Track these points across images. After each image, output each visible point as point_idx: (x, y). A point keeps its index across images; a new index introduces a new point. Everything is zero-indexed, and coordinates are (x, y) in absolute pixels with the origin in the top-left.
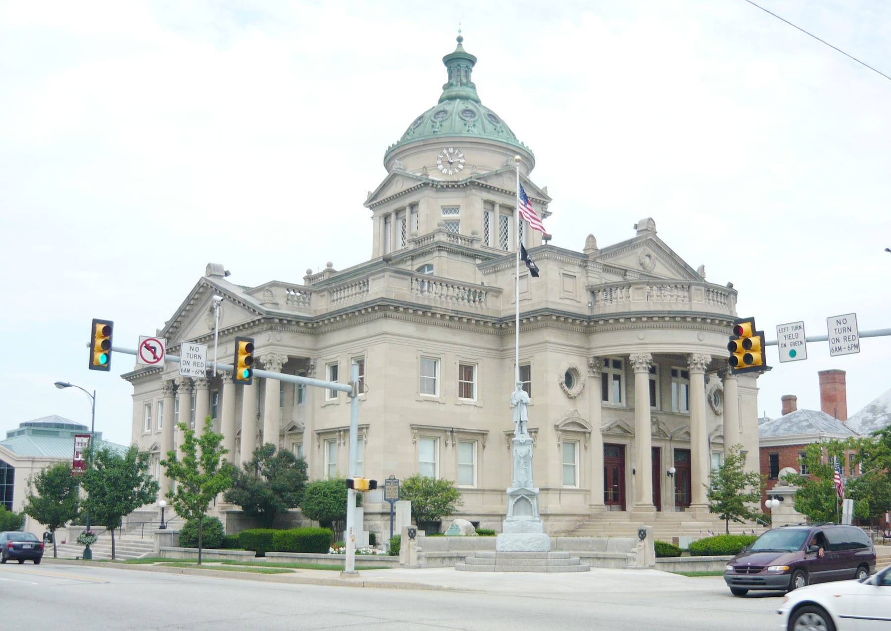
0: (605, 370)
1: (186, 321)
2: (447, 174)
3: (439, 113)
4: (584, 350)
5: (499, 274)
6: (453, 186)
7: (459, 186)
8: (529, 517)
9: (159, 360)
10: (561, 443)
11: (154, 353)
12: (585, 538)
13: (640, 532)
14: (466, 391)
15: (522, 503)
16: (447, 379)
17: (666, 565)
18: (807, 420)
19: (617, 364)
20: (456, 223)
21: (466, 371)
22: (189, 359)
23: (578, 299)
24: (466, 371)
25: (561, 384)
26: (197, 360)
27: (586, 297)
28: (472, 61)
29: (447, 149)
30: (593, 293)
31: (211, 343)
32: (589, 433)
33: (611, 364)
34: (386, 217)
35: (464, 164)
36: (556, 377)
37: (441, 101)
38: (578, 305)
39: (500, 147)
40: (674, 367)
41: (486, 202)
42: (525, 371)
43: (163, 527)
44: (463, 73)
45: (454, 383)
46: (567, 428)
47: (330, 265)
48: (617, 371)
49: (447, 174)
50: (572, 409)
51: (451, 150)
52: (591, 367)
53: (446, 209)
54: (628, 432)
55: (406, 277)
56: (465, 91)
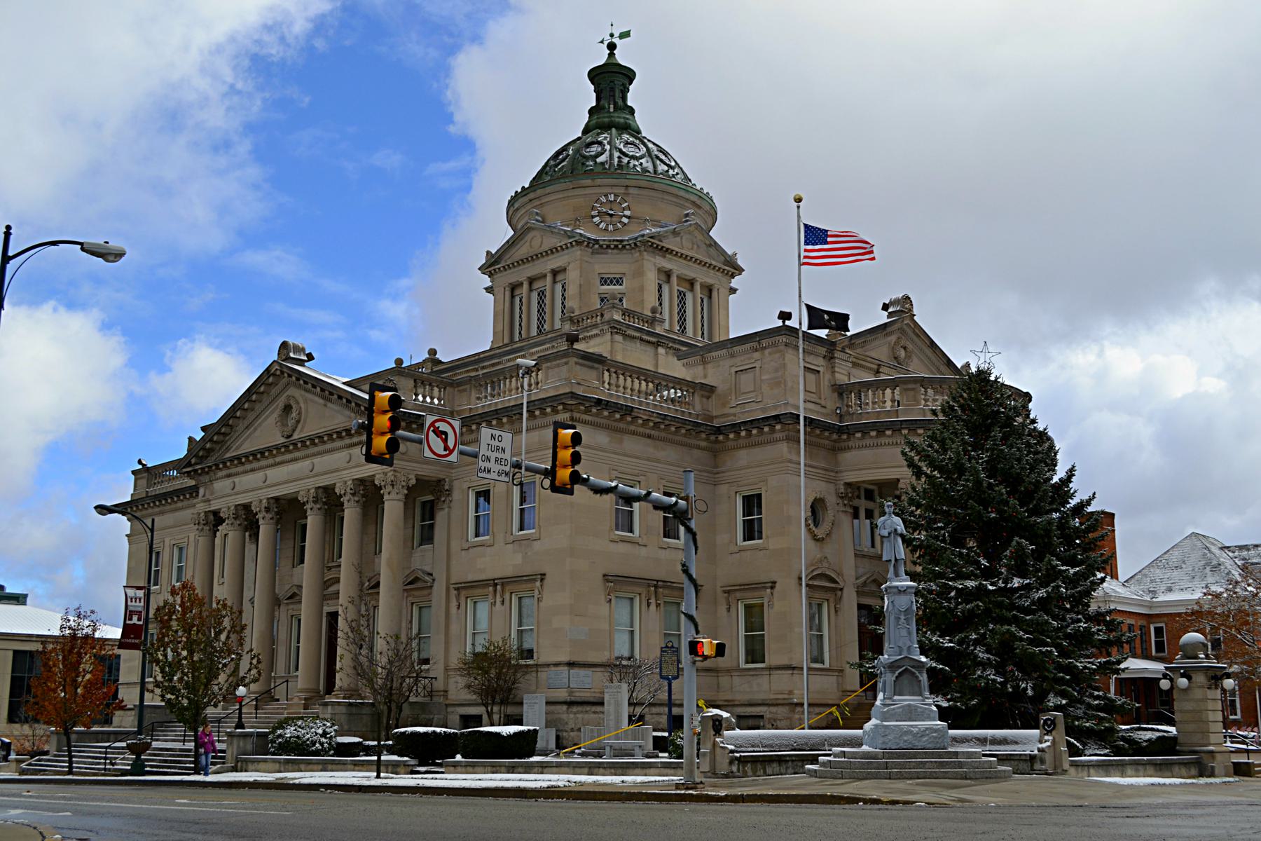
0: (856, 502)
1: (241, 425)
2: (606, 229)
4: (831, 474)
6: (616, 247)
7: (624, 247)
9: (451, 452)
11: (445, 441)
17: (1140, 768)
22: (489, 453)
23: (823, 403)
26: (500, 456)
27: (831, 402)
28: (629, 75)
30: (841, 395)
31: (516, 426)
32: (841, 589)
34: (514, 288)
35: (629, 217)
37: (586, 131)
38: (823, 410)
42: (752, 503)
43: (240, 725)
44: (618, 94)
46: (816, 583)
47: (433, 352)
49: (606, 229)
52: (841, 497)
55: (596, 365)
56: (620, 118)
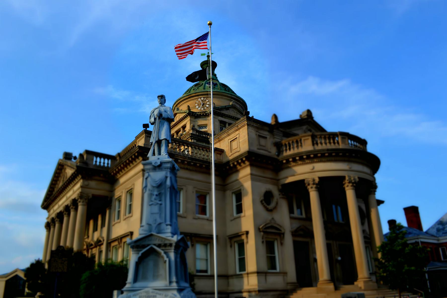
4: (275, 181)
5: (221, 142)
12: (212, 110)
23: (269, 150)
29: (200, 98)
39: (228, 97)
41: (221, 122)
45: (194, 203)
50: (270, 218)
51: (202, 99)
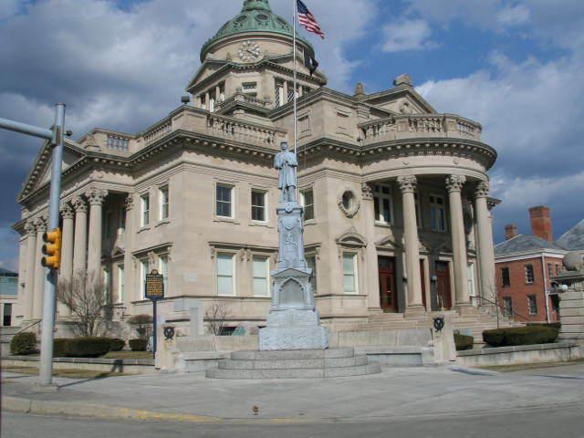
0: (377, 195)
3: (241, 19)
8: (301, 306)
10: (341, 254)
13: (436, 320)
14: (258, 214)
15: (291, 285)
16: (240, 202)
18: (528, 241)
19: (385, 191)
20: (255, 95)
21: (257, 197)
24: (257, 197)
25: (339, 204)
27: (358, 133)
33: (381, 190)
36: (334, 197)
40: (432, 195)
48: (386, 196)
50: (349, 225)
53: (246, 85)
54: (399, 247)
